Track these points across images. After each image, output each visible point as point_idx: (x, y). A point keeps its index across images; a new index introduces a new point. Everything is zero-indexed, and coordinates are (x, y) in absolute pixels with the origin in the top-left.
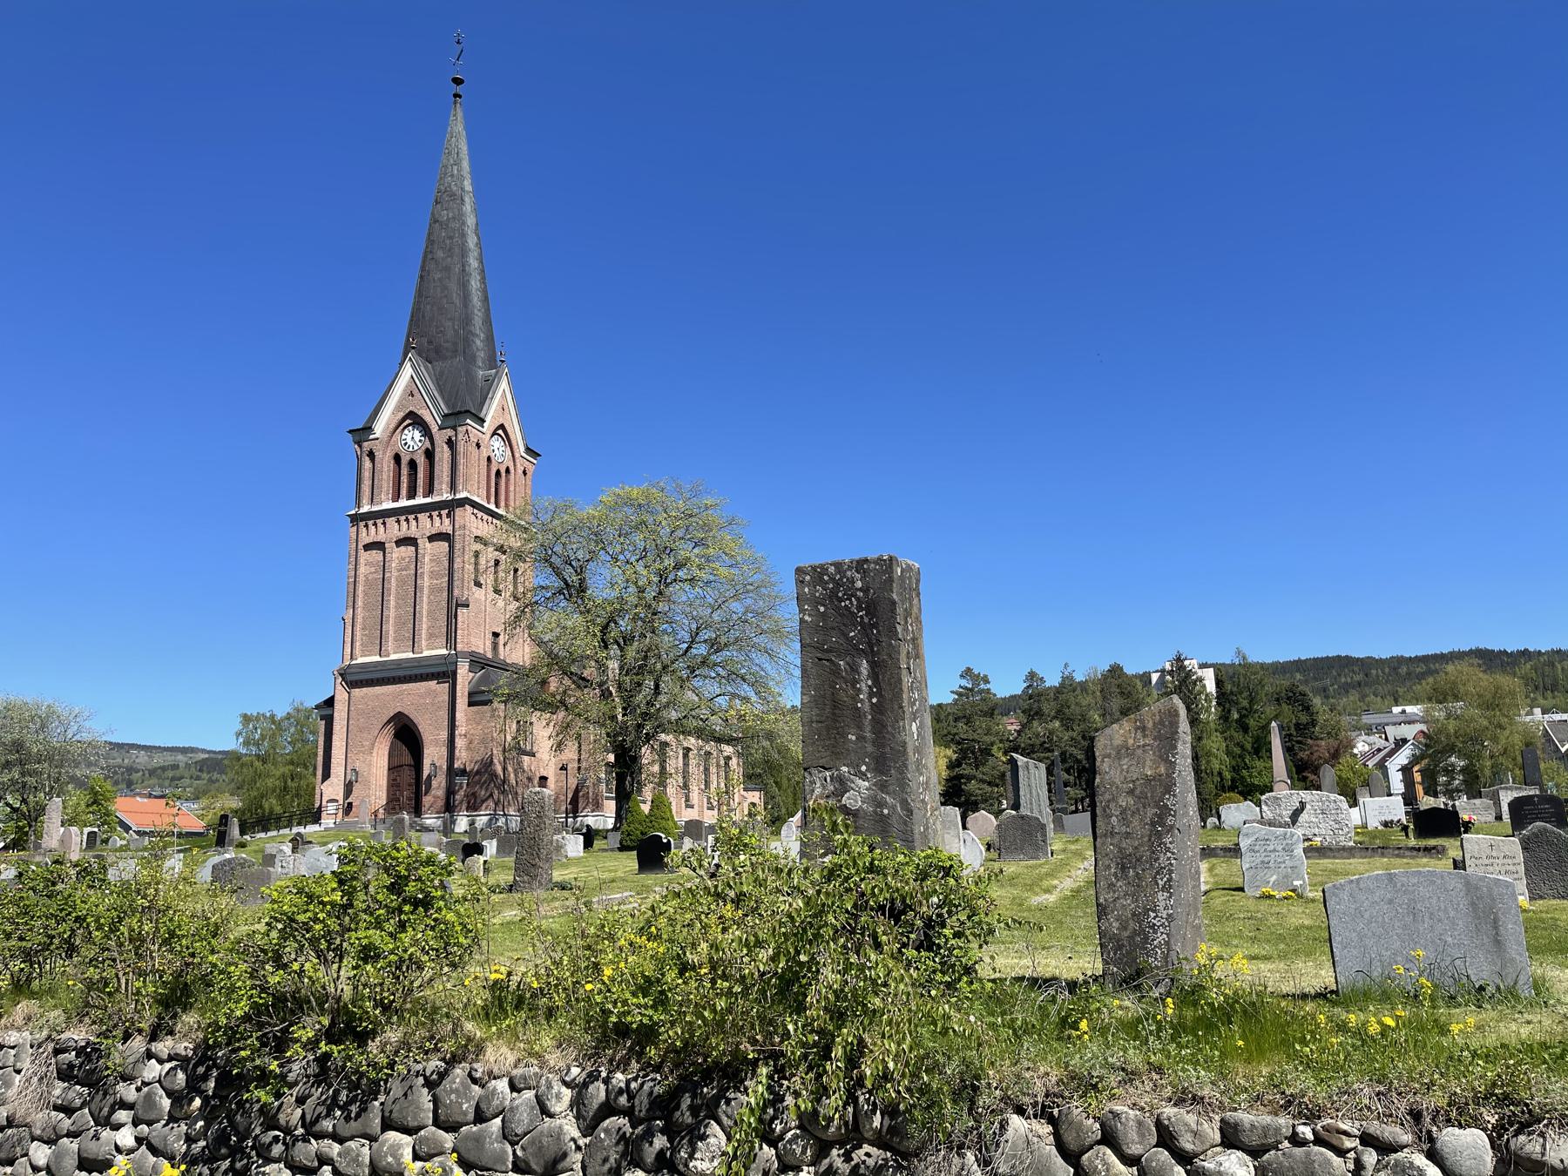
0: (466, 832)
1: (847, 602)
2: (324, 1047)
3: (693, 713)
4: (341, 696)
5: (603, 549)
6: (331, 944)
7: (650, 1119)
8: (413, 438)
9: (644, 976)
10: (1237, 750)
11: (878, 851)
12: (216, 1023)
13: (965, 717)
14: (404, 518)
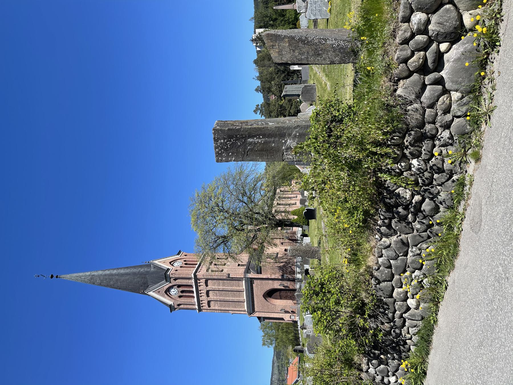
0: (301, 275)
1: (228, 145)
2: (366, 316)
3: (266, 201)
4: (257, 314)
5: (211, 230)
6: (334, 315)
7: (393, 212)
8: (173, 292)
9: (348, 214)
10: (283, 22)
11: (310, 136)
12: (357, 350)
13: (270, 113)
14: (200, 295)
